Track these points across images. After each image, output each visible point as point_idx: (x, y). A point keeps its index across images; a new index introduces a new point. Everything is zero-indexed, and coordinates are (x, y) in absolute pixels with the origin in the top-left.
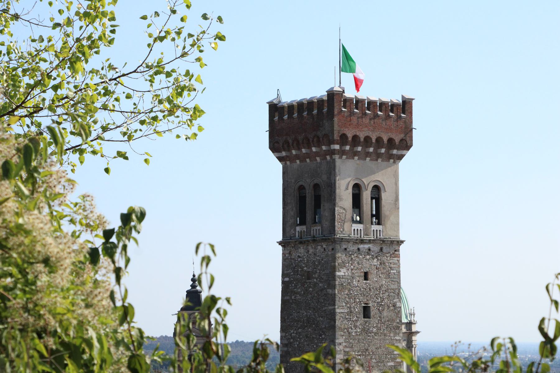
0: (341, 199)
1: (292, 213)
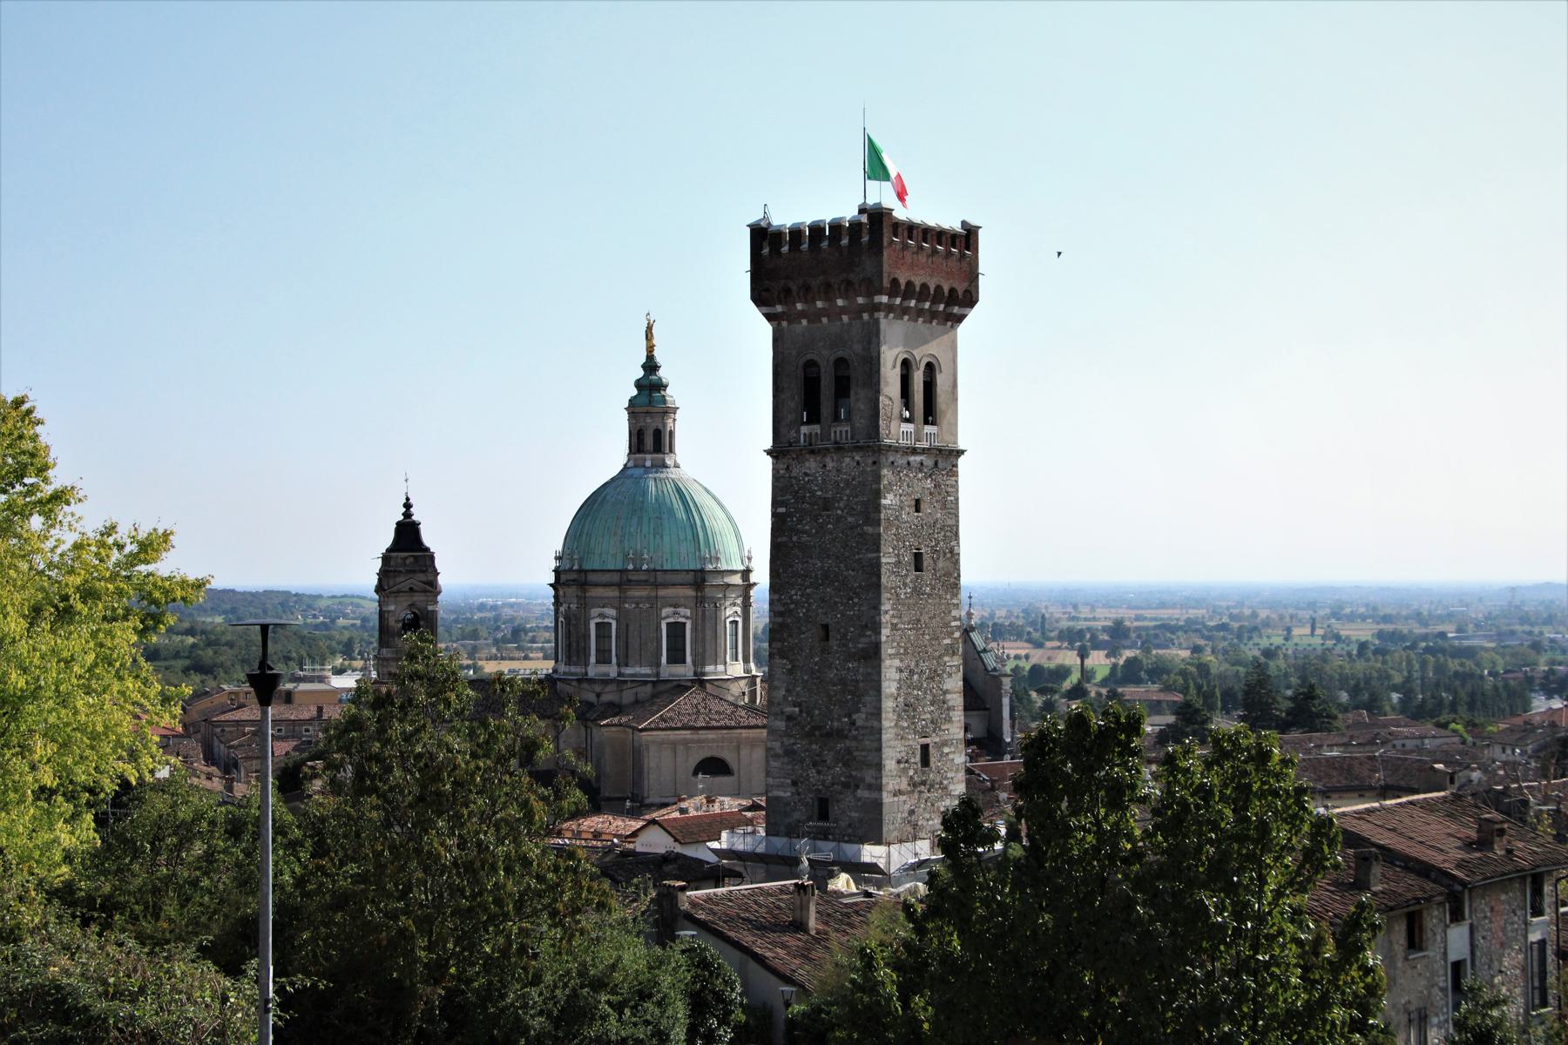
0: (887, 384)
1: (792, 405)
